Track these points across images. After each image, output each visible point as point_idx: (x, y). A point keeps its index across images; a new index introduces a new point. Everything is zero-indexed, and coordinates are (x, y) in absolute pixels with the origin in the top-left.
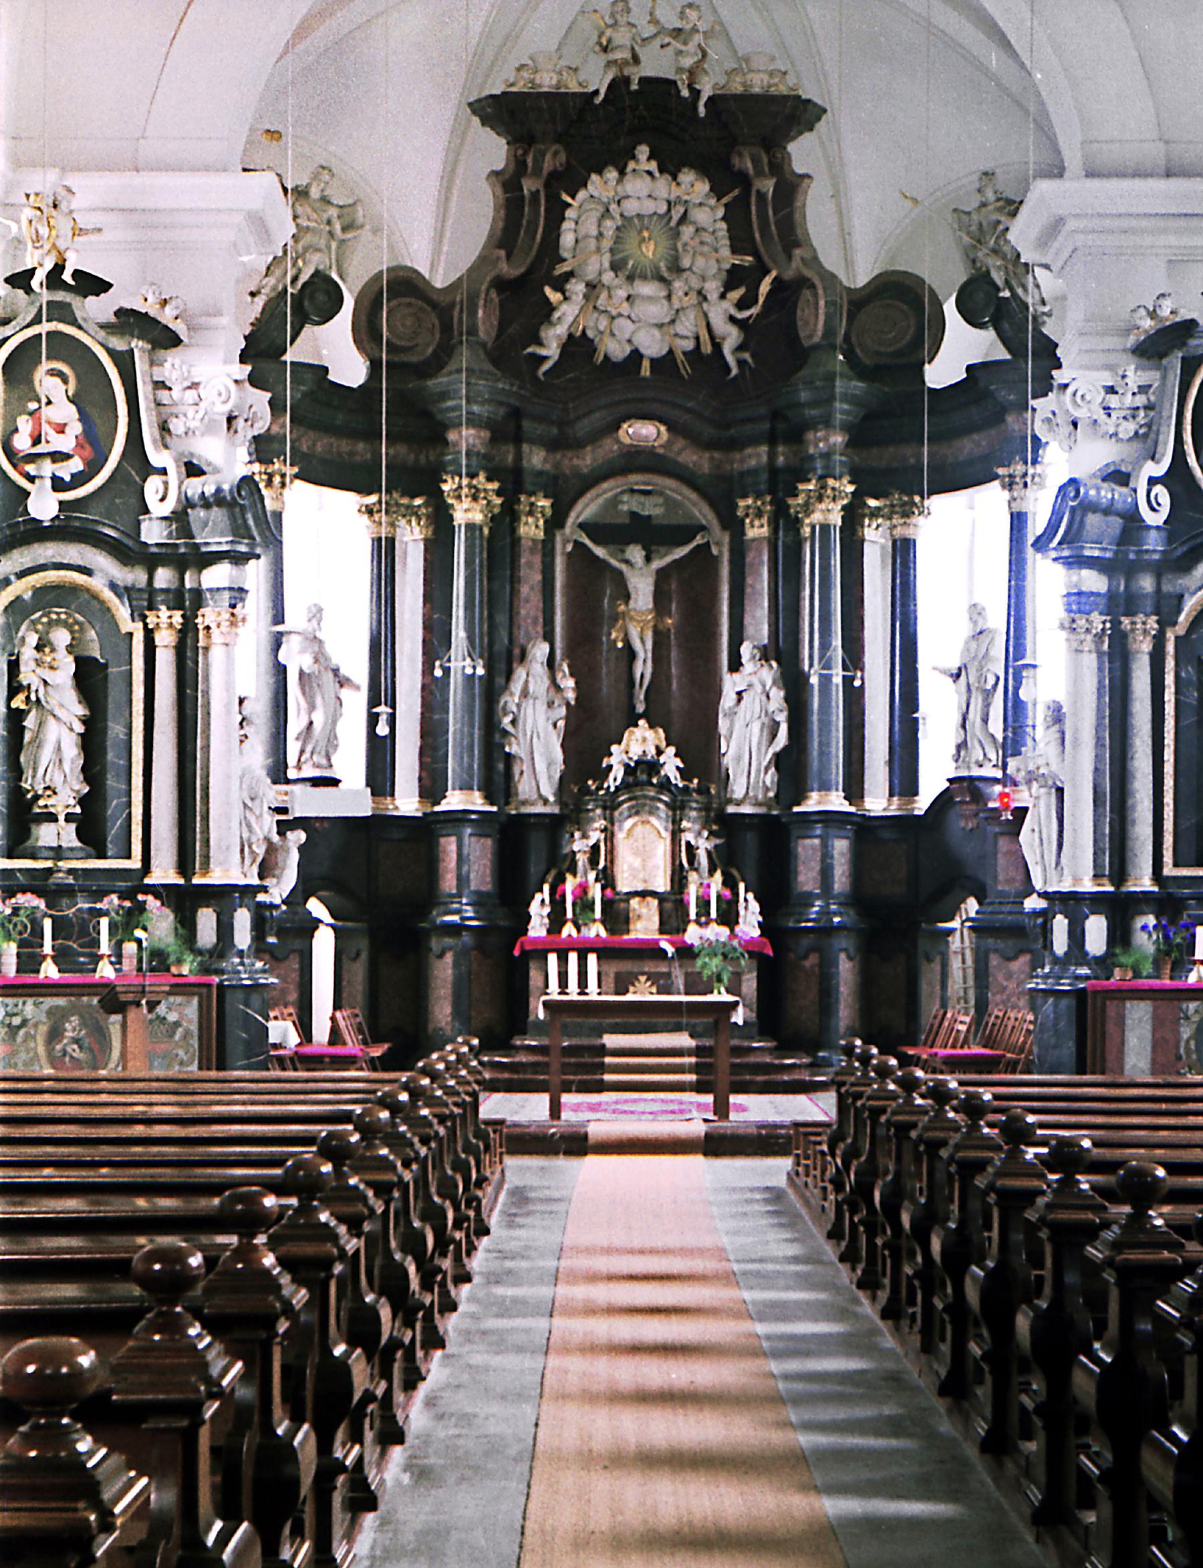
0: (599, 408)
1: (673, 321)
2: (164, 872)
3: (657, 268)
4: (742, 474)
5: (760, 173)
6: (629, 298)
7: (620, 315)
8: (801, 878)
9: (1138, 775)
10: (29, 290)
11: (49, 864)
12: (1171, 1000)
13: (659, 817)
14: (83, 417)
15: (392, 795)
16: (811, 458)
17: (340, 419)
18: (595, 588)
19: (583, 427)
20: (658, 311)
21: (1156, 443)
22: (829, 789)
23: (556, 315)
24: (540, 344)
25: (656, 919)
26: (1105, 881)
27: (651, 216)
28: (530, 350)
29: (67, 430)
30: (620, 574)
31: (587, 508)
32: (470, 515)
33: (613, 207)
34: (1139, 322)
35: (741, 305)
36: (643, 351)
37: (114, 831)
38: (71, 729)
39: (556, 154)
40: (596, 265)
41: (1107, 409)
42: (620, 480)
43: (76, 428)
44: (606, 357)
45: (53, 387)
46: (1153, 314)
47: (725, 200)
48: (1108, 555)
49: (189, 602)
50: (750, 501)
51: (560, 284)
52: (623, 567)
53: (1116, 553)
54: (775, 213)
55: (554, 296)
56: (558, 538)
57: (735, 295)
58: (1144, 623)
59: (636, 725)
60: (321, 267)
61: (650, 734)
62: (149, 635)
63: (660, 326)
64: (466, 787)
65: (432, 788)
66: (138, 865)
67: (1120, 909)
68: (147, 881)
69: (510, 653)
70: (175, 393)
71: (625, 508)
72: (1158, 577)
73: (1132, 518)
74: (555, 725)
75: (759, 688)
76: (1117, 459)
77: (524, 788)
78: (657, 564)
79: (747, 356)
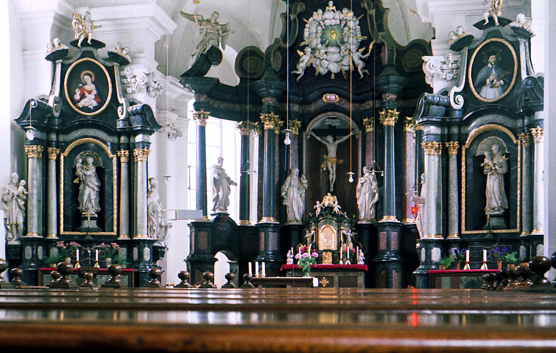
0: (316, 90)
1: (341, 60)
2: (124, 236)
3: (337, 43)
4: (365, 111)
5: (370, 8)
6: (326, 53)
7: (323, 59)
8: (381, 245)
9: (452, 198)
10: (77, 46)
11: (85, 233)
12: (456, 276)
13: (333, 225)
14: (97, 88)
15: (248, 219)
16: (384, 103)
17: (229, 97)
18: (318, 151)
19: (311, 96)
20: (336, 57)
21: (459, 80)
22: (390, 215)
23: (301, 60)
24: (297, 70)
25: (331, 259)
26: (441, 236)
27: (335, 25)
28: (293, 72)
29: (92, 93)
30: (325, 145)
31: (315, 124)
32: (268, 126)
33: (321, 22)
34: (452, 38)
35: (364, 53)
36: (332, 71)
37: (108, 222)
38: (94, 190)
39: (301, 6)
40: (316, 42)
41: (442, 70)
42: (324, 114)
43: (95, 92)
44: (319, 73)
45: (88, 80)
46: (456, 35)
47: (359, 18)
48: (439, 120)
49: (130, 147)
50: (366, 120)
51: (302, 49)
52: (326, 143)
53: (442, 119)
54: (376, 22)
55: (301, 53)
56: (304, 134)
57: (361, 50)
58: (453, 144)
59: (327, 195)
60: (214, 45)
61: (332, 198)
62: (119, 159)
63: (337, 62)
64: (268, 216)
65: (260, 218)
66: (116, 234)
67: (445, 246)
68: (118, 239)
69: (287, 172)
70: (128, 80)
71: (327, 123)
72: (460, 128)
73: (448, 109)
74: (301, 196)
75: (369, 182)
76: (446, 87)
77: (290, 216)
78: (337, 142)
79: (366, 71)
